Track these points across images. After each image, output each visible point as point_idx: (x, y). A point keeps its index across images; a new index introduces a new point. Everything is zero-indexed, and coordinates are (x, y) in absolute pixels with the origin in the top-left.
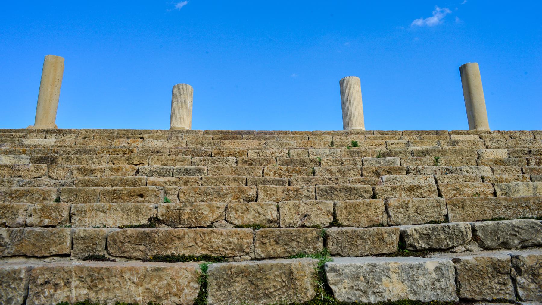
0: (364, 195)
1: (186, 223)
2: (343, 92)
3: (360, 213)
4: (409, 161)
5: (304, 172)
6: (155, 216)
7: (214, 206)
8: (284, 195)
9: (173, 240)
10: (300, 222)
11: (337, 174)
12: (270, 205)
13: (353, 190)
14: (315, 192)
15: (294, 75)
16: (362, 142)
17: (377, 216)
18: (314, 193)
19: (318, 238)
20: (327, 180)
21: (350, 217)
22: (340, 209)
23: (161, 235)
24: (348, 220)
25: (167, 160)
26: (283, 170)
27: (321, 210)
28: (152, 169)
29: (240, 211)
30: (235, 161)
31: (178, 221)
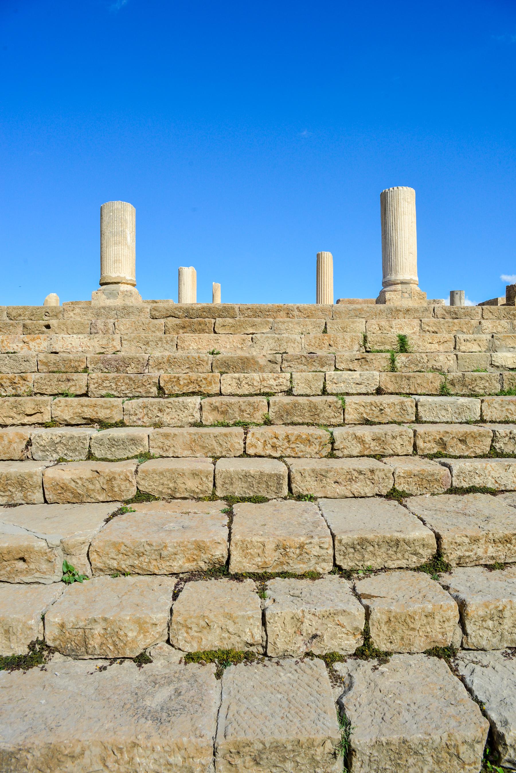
0: (421, 551)
1: (98, 651)
2: (385, 214)
3: (413, 629)
4: (496, 405)
5: (316, 441)
6: (41, 638)
7: (146, 623)
8: (277, 554)
9: (63, 762)
10: (304, 649)
11: (373, 444)
12: (249, 618)
13: (402, 543)
14: (334, 548)
15: (305, 133)
16: (415, 337)
17: (443, 634)
18: (331, 551)
19: (335, 755)
20: (356, 474)
21: (396, 637)
22: (376, 624)
23: (37, 754)
24: (391, 642)
25: (82, 406)
26: (280, 438)
27: (343, 627)
28: (54, 438)
29: (195, 628)
30: (198, 406)
31: (83, 649)
